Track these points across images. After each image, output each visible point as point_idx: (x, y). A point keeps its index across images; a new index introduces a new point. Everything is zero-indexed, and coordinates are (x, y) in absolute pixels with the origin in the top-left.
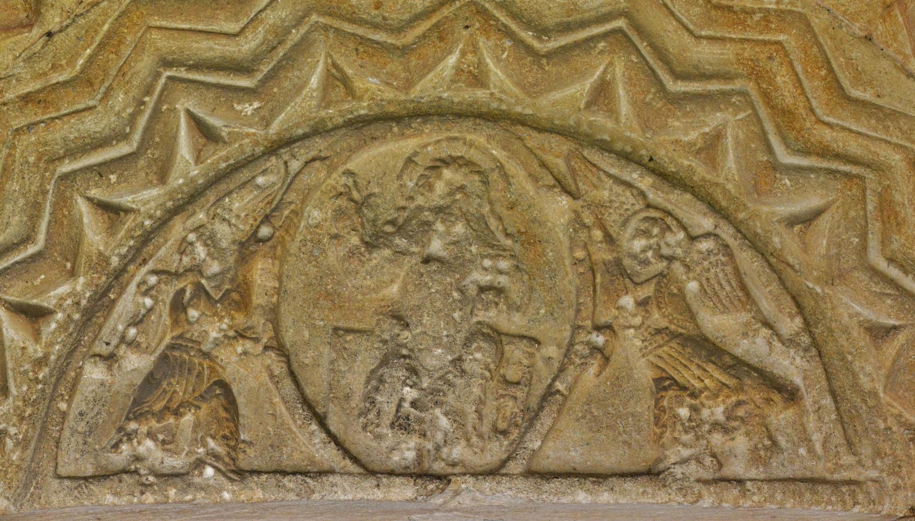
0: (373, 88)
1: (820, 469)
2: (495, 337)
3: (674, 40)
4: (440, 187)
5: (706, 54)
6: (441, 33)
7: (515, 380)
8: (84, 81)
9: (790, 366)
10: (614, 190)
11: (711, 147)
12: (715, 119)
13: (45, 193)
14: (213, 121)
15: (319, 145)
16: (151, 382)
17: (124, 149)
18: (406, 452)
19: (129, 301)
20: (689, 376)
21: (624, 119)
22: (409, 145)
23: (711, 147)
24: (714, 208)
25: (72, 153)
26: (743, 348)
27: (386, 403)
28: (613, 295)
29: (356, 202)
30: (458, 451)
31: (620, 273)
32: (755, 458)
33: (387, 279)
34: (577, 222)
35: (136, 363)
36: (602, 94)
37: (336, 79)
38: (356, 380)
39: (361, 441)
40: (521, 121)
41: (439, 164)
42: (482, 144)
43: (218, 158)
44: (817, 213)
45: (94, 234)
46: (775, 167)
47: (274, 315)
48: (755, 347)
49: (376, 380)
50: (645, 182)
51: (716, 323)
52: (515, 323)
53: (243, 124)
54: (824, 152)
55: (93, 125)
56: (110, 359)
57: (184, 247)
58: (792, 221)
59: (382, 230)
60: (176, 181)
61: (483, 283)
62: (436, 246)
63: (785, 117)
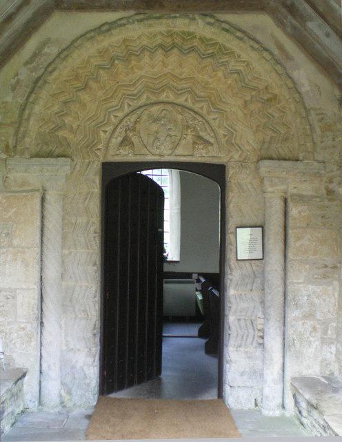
0: (153, 99)
1: (215, 155)
2: (170, 136)
3: (197, 92)
4: (163, 114)
5: (202, 94)
6: (164, 90)
7: (282, 204)
8: (112, 97)
9: (212, 140)
10: (188, 115)
11: (202, 108)
12: (203, 104)
13: (324, 50)
14: (131, 103)
15: (145, 108)
16: (122, 142)
17: (117, 108)
18: (158, 152)
19: (118, 130)
20: (198, 142)
21: (189, 104)
22: (159, 107)
23: (202, 108)
24: (202, 117)
25: (110, 108)
26: (205, 138)
27: (155, 145)
28: (187, 130)
29: (150, 116)
30: (165, 152)
31: (188, 127)
32: (206, 153)
33: (155, 127)
34: (183, 119)
35: (120, 139)
36: (186, 100)
37: (148, 98)
38: (151, 141)
39: (151, 150)
40: (174, 104)
41: (162, 111)
42: (169, 107)
43: (131, 109)
44: (216, 119)
45: (113, 118)
46: (211, 111)
47: (139, 132)
48: (207, 138)
49: (154, 142)
50: (192, 113)
51: (201, 134)
52: (174, 133)
53: (135, 104)
54: (219, 109)
55: (114, 104)
56: (116, 138)
57: (126, 122)
58: (213, 119)
59: (156, 120)
60: (125, 112)
61: (47, 85)
62: (163, 122)
63: (213, 104)
